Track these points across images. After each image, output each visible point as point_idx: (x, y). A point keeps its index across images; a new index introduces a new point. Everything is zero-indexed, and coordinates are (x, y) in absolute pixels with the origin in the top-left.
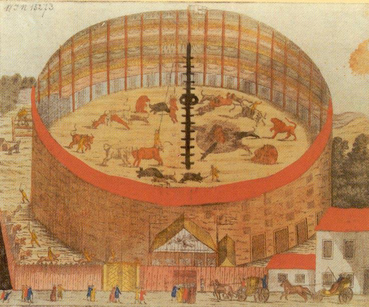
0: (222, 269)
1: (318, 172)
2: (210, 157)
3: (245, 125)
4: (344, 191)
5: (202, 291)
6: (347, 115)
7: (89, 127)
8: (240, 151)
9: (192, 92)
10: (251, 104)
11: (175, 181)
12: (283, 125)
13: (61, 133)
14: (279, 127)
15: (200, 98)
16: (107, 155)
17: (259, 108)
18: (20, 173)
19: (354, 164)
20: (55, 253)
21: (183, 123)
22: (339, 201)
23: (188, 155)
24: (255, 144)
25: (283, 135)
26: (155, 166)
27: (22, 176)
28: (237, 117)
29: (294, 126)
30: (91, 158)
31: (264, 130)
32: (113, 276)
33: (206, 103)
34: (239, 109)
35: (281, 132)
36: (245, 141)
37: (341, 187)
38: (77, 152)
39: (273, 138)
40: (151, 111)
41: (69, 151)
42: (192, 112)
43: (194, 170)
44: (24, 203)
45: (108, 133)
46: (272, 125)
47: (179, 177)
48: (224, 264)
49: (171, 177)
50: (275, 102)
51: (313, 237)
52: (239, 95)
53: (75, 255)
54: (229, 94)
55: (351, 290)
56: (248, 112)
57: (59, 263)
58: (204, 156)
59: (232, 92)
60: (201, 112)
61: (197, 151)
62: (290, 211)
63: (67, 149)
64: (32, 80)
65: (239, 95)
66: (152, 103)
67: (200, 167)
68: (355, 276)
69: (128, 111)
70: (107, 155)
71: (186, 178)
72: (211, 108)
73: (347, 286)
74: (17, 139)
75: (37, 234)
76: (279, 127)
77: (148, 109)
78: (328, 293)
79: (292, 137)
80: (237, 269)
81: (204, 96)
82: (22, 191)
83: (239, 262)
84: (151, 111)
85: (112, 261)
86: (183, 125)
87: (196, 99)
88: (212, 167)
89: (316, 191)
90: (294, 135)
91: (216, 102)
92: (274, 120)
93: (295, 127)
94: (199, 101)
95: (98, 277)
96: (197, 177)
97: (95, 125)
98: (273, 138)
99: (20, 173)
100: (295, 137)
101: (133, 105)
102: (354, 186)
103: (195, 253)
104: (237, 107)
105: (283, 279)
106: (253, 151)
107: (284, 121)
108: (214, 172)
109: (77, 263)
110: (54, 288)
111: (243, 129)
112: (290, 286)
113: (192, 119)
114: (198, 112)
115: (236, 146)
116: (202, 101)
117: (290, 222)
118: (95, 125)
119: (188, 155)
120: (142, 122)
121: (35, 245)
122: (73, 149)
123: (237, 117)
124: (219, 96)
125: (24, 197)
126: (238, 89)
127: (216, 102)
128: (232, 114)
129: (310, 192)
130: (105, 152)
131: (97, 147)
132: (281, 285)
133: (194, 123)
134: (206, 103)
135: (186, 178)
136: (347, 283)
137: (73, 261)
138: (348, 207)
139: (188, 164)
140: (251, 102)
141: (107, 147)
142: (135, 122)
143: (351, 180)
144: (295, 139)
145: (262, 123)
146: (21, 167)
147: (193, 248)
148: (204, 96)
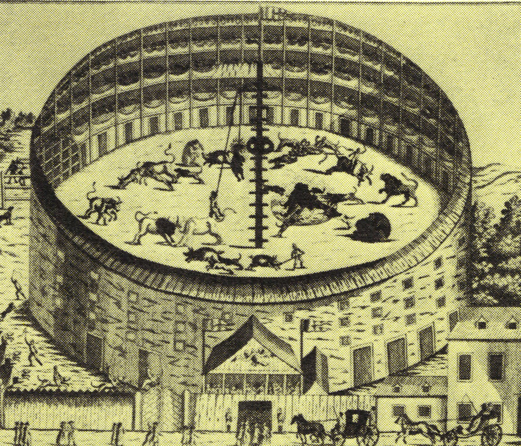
0: (309, 398)
1: (451, 252)
2: (291, 230)
3: (341, 183)
4: (489, 280)
5: (280, 431)
6: (493, 167)
7: (114, 187)
8: (335, 222)
9: (265, 134)
10: (351, 152)
11: (241, 268)
12: (398, 183)
13: (73, 193)
14: (392, 186)
15: (276, 143)
16: (140, 229)
17: (362, 158)
18: (13, 255)
19: (94, 286)
20: (63, 374)
21: (251, 181)
22: (481, 296)
23: (259, 228)
24: (359, 212)
25: (399, 199)
26: (212, 244)
27: (15, 259)
28: (329, 172)
29: (413, 184)
30: (116, 232)
31: (371, 191)
32: (150, 409)
33: (286, 150)
34: (332, 161)
35: (397, 194)
36: (341, 207)
37: (483, 275)
38: (97, 223)
39: (384, 202)
40: (204, 164)
41: (84, 222)
42: (265, 164)
43: (267, 250)
44: (18, 299)
45: (147, 199)
46: (382, 184)
47: (246, 262)
48: (311, 391)
49: (235, 262)
50: (387, 150)
51: (444, 351)
52: (333, 138)
53: (93, 378)
54: (318, 137)
55: (500, 428)
56: (345, 165)
57: (69, 389)
58: (283, 229)
59: (322, 134)
60: (278, 163)
61: (272, 223)
62: (410, 311)
63: (81, 220)
64: (30, 117)
65: (333, 138)
66: (207, 151)
67: (278, 247)
68: (505, 408)
69: (171, 163)
70: (140, 229)
71: (256, 261)
72: (291, 159)
73: (493, 421)
74: (8, 204)
75: (37, 346)
76: (392, 186)
77: (200, 160)
78: (465, 432)
79: (412, 202)
80: (331, 397)
81: (282, 140)
82: (15, 282)
83: (334, 388)
84: (204, 164)
85: (147, 387)
86: (250, 231)
87: (271, 144)
88: (294, 246)
89: (449, 281)
90: (415, 199)
91: (300, 150)
92: (386, 177)
93: (416, 187)
94: (275, 148)
95: (128, 409)
96: (271, 262)
97: (122, 183)
98: (384, 202)
99: (13, 255)
100: (416, 201)
101: (178, 151)
102: (503, 273)
103: (270, 375)
104: (329, 156)
105: (399, 412)
106: (353, 222)
107: (399, 177)
108: (296, 253)
109: (97, 389)
110: (63, 424)
111: (337, 190)
112: (410, 423)
113: (265, 175)
114: (273, 165)
115: (333, 214)
116: (279, 149)
117: (410, 328)
118: (122, 183)
119: (259, 228)
120: (192, 180)
121: (35, 363)
122: (90, 220)
123: (329, 172)
124: (304, 140)
125: (19, 290)
126: (331, 131)
127: (300, 150)
128: (324, 168)
129: (439, 284)
130: (137, 224)
131: (125, 213)
132: (396, 422)
133: (267, 181)
134: (286, 150)
135: (256, 261)
136: (494, 417)
137: (90, 386)
138: (495, 305)
139: (259, 241)
140: (350, 150)
141: (140, 217)
142: (181, 179)
143: (500, 265)
144: (416, 205)
145: (367, 181)
146: (13, 245)
147: (267, 368)
148: (282, 140)
